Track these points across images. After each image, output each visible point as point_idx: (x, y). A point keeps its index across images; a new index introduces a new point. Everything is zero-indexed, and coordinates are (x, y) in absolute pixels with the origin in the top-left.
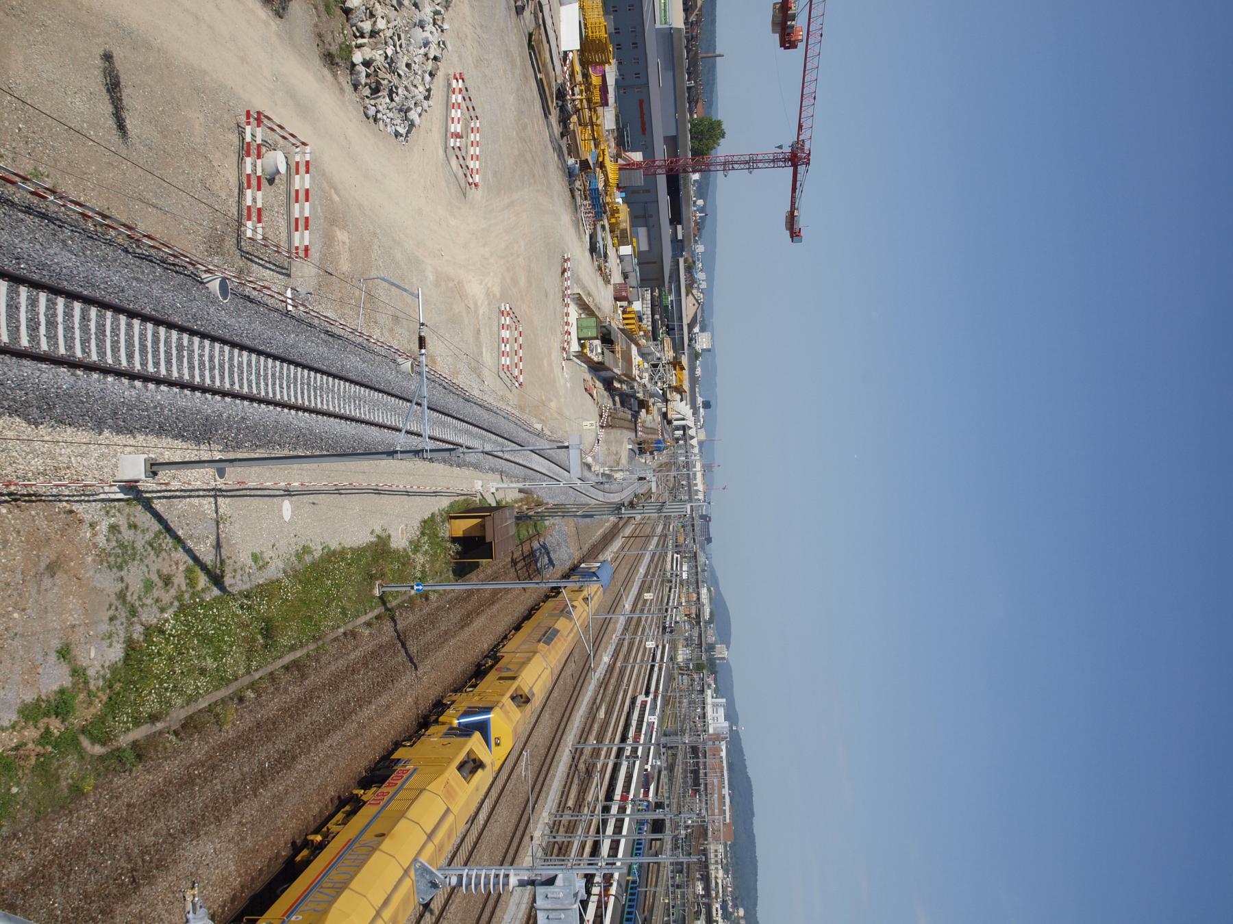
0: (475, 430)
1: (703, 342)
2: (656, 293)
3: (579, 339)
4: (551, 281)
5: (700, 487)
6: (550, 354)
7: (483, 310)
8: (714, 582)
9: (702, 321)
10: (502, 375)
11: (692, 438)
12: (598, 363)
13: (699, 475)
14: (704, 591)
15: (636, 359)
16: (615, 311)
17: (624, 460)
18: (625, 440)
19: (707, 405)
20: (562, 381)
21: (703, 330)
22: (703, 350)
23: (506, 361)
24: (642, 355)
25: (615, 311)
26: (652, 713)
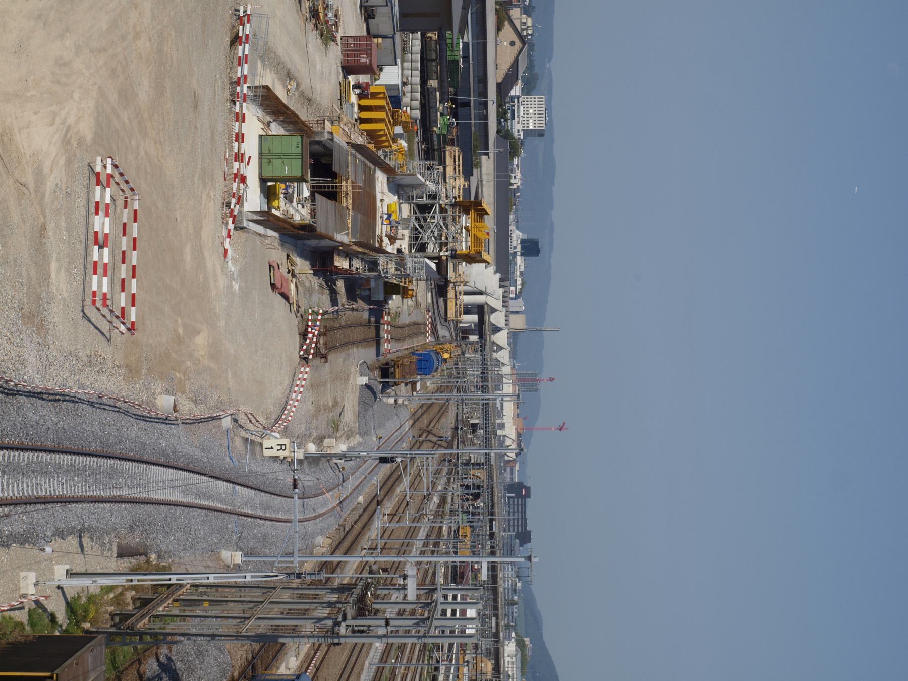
0: (26, 456)
1: (528, 115)
2: (433, 36)
3: (263, 180)
4: (207, 70)
6: (198, 230)
7: (55, 178)
8: (533, 623)
9: (528, 75)
11: (497, 330)
12: (302, 227)
13: (509, 408)
14: (510, 648)
15: (385, 198)
16: (343, 98)
17: (349, 416)
18: (354, 369)
19: (531, 248)
20: (222, 282)
21: (527, 91)
22: (527, 133)
23: (101, 284)
24: (397, 188)
25: (343, 98)
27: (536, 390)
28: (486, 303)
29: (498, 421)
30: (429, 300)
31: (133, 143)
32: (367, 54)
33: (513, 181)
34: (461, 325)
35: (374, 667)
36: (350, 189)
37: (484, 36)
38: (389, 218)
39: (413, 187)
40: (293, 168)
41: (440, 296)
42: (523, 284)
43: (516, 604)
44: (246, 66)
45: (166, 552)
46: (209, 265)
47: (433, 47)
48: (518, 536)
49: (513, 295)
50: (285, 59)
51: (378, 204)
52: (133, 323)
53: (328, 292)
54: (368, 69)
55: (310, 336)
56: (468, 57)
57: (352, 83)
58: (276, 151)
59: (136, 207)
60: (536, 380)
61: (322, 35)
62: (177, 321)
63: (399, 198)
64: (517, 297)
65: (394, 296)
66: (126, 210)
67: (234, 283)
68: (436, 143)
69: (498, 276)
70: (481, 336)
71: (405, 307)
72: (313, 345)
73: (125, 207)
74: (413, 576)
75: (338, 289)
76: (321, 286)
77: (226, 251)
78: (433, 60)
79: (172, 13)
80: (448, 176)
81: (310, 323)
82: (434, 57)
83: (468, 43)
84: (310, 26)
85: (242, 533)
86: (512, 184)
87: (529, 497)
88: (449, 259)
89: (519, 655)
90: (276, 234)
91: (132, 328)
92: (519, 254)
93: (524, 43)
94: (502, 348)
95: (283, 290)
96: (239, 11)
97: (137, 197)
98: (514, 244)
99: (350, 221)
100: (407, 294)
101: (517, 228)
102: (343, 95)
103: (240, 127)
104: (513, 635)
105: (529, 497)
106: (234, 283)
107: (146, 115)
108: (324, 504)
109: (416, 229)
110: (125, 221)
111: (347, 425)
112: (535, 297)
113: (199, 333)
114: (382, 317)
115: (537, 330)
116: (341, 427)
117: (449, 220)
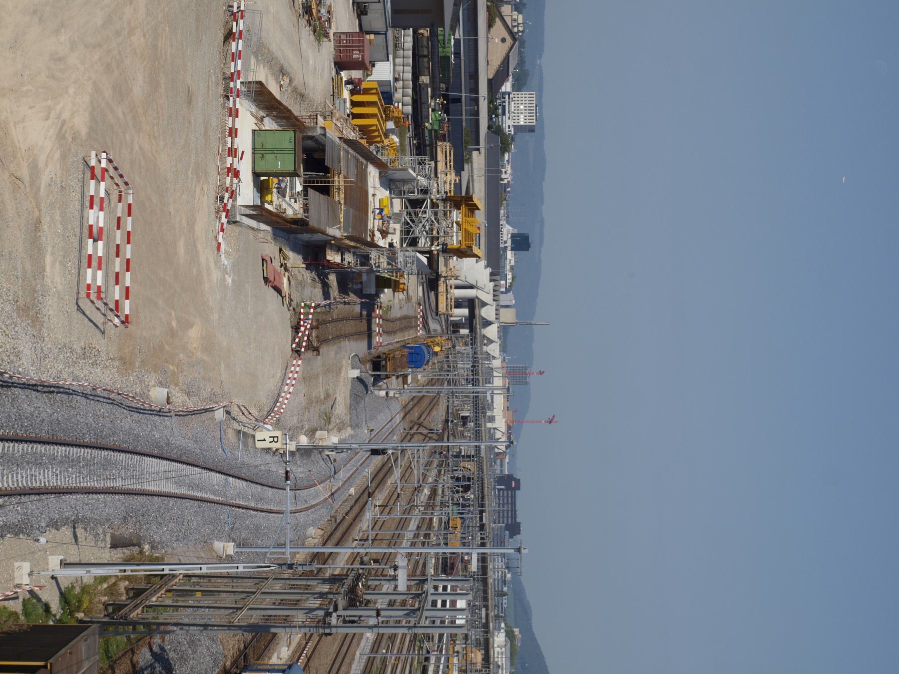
1: (519, 111)
2: (425, 32)
3: (256, 175)
4: (202, 66)
5: (500, 423)
6: (191, 223)
7: (49, 172)
9: (519, 71)
10: (86, 305)
11: (487, 323)
12: (295, 221)
13: (499, 402)
14: (499, 639)
15: (377, 193)
17: (341, 409)
18: (346, 362)
19: (521, 243)
20: (216, 275)
21: (518, 86)
22: (518, 128)
24: (388, 182)
25: (335, 94)
26: (244, 567)
27: (526, 383)
28: (477, 297)
30: (421, 294)
31: (127, 137)
32: (359, 50)
33: (503, 176)
34: (452, 319)
35: (365, 657)
36: (342, 183)
39: (404, 182)
40: (285, 163)
41: (431, 290)
42: (513, 278)
43: (505, 594)
44: (239, 62)
45: (159, 543)
46: (203, 259)
47: (425, 43)
48: (508, 527)
49: (503, 290)
50: (278, 53)
51: (370, 198)
52: (127, 316)
53: (320, 286)
55: (302, 329)
56: (460, 53)
57: (344, 79)
58: (269, 146)
59: (130, 201)
60: (526, 374)
61: (315, 31)
62: (170, 314)
63: (390, 193)
65: (386, 290)
66: (121, 204)
67: (227, 276)
68: (427, 138)
69: (489, 270)
70: (472, 329)
71: (396, 301)
72: (306, 338)
73: (120, 201)
74: (403, 567)
76: (313, 280)
77: (219, 244)
78: (425, 56)
79: (166, 9)
81: (302, 317)
82: (426, 53)
83: (459, 40)
86: (502, 180)
88: (441, 253)
90: (268, 228)
91: (126, 321)
92: (509, 248)
93: (514, 39)
94: (492, 342)
95: (276, 283)
96: (232, 7)
97: (131, 191)
98: (505, 239)
99: (342, 215)
100: (399, 288)
101: (508, 223)
103: (233, 122)
104: (503, 625)
106: (227, 276)
107: (140, 110)
109: (408, 224)
110: (119, 215)
112: (525, 291)
114: (374, 311)
115: (527, 324)
116: (333, 419)
117: (441, 215)
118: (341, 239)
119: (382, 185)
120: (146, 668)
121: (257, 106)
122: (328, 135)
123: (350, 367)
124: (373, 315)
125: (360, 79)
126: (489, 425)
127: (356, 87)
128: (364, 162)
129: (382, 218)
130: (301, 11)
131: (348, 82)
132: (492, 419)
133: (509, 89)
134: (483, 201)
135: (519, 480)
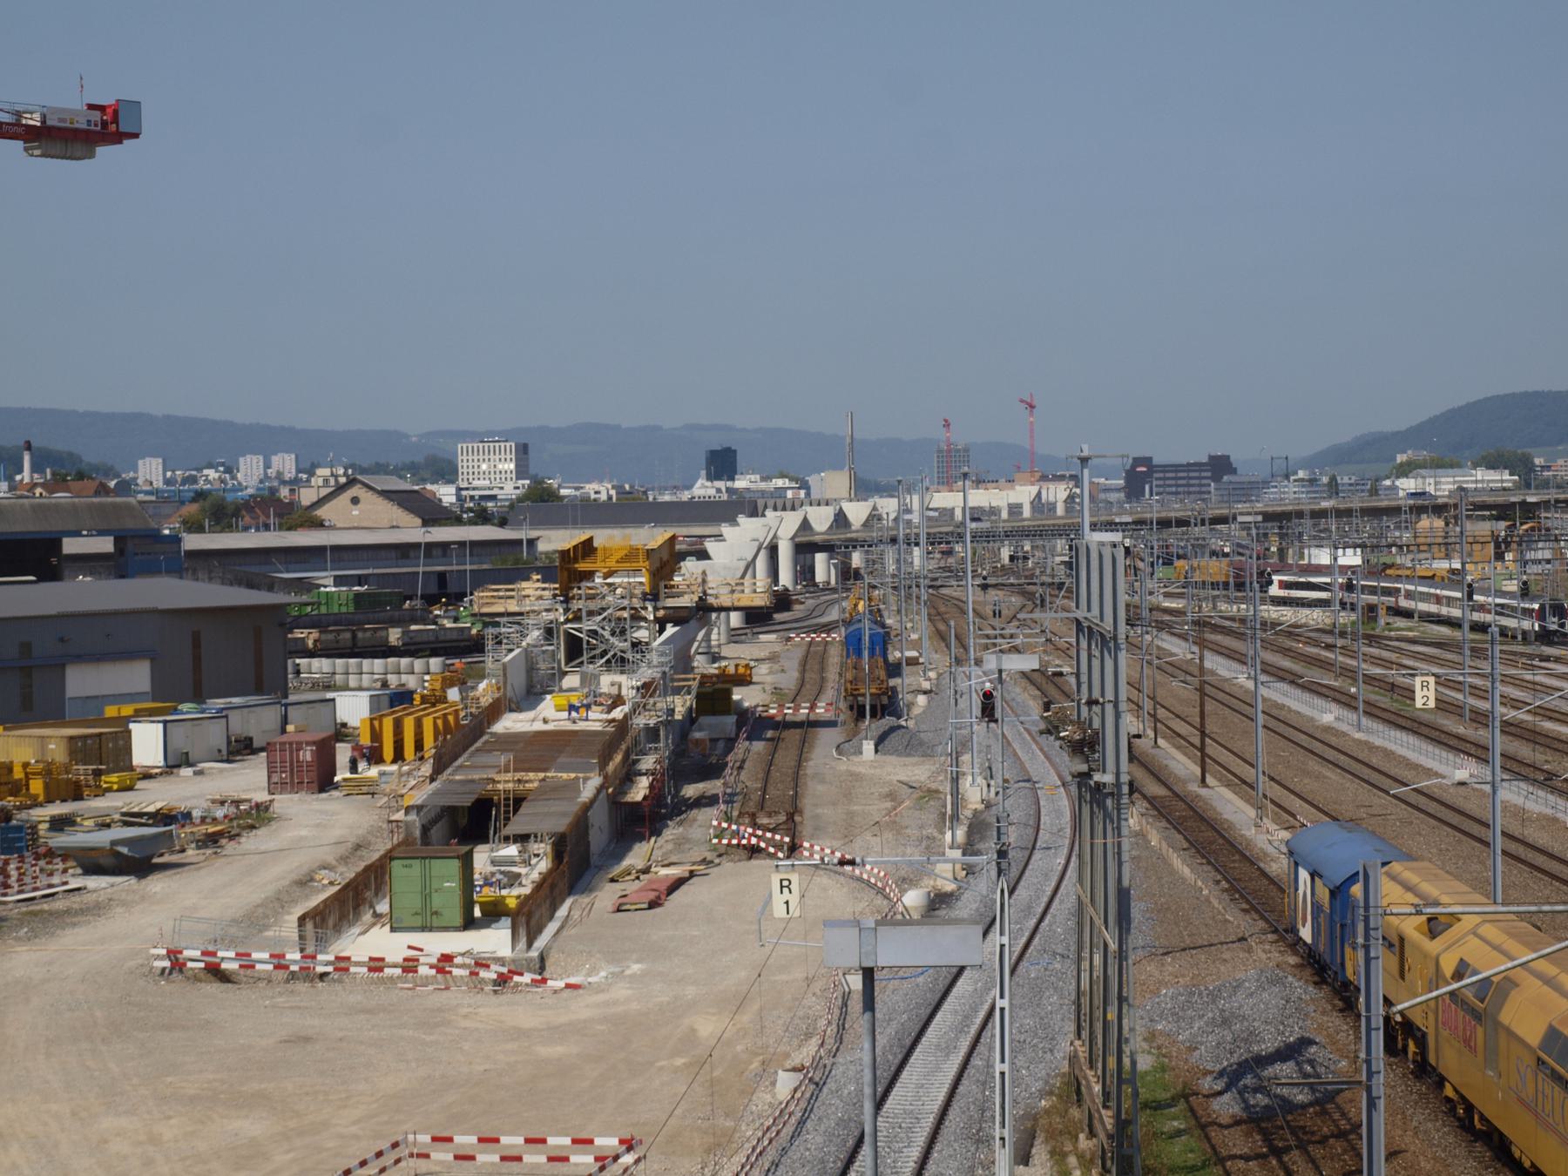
1: (492, 472)
2: (310, 637)
3: (469, 923)
6: (520, 1034)
11: (841, 520)
12: (558, 855)
13: (980, 498)
15: (548, 715)
16: (369, 789)
17: (917, 771)
18: (844, 765)
19: (722, 463)
20: (621, 991)
21: (446, 471)
22: (521, 472)
24: (532, 694)
25: (369, 789)
27: (966, 450)
28: (792, 539)
29: (1004, 515)
30: (772, 637)
31: (331, 1144)
32: (298, 750)
33: (603, 497)
34: (833, 582)
35: (1365, 721)
36: (509, 776)
37: (318, 551)
38: (577, 709)
39: (531, 668)
40: (446, 873)
41: (771, 618)
42: (782, 476)
43: (1333, 479)
44: (255, 956)
45: (1047, 1082)
46: (585, 1014)
47: (330, 637)
48: (1217, 478)
49: (802, 493)
50: (270, 890)
51: (550, 727)
52: (622, 1142)
53: (695, 811)
54: (325, 752)
55: (754, 841)
56: (359, 576)
57: (348, 775)
58: (417, 903)
59: (427, 1138)
60: (949, 451)
61: (252, 827)
62: (661, 1068)
63: (550, 692)
64: (804, 485)
65: (735, 697)
66: (433, 1155)
67: (628, 972)
69: (741, 519)
70: (854, 544)
71: (769, 679)
72: (769, 835)
73: (427, 1156)
74: (999, 660)
75: (697, 794)
76: (680, 824)
77: (568, 986)
78: (354, 637)
79: (135, 1081)
80: (517, 609)
81: (735, 842)
82: (348, 635)
83: (336, 577)
84: (229, 847)
85: (1055, 954)
86: (610, 498)
87: (1150, 459)
89: (1423, 472)
90: (568, 902)
91: (629, 1145)
92: (729, 484)
93: (352, 482)
94: (875, 508)
95: (663, 887)
96: (164, 969)
97: (411, 1137)
98: (712, 492)
99: (565, 776)
100: (744, 675)
101: (689, 487)
102: (365, 789)
103: (358, 964)
104: (1388, 483)
105: (1150, 459)
106: (628, 972)
107: (292, 1124)
108: (1058, 813)
109: (608, 661)
110: (450, 1157)
111: (933, 776)
112: (798, 458)
113: (693, 1030)
114: (772, 717)
115: (852, 450)
116: (934, 786)
117: (593, 605)
118: (606, 777)
119: (532, 707)
120: (1245, 1101)
121: (351, 924)
122: (419, 802)
123: (855, 759)
124: (779, 718)
125: (354, 749)
126: (1027, 512)
127: (364, 756)
128: (485, 738)
129: (588, 707)
130: (209, 851)
131: (354, 768)
132: (1015, 509)
133: (451, 489)
134: (577, 532)
135: (1135, 459)
